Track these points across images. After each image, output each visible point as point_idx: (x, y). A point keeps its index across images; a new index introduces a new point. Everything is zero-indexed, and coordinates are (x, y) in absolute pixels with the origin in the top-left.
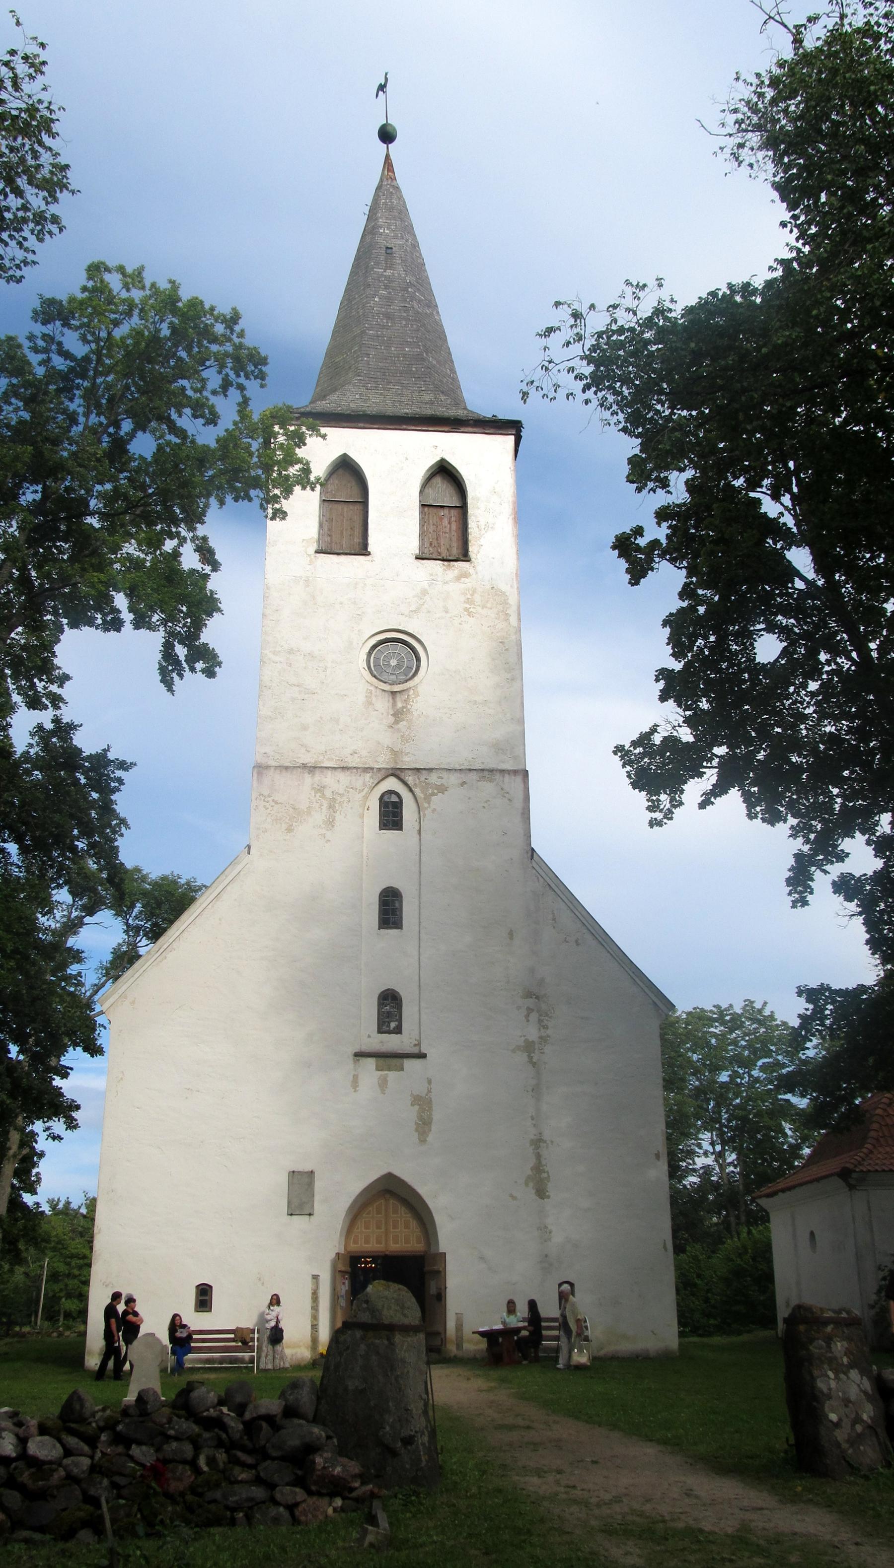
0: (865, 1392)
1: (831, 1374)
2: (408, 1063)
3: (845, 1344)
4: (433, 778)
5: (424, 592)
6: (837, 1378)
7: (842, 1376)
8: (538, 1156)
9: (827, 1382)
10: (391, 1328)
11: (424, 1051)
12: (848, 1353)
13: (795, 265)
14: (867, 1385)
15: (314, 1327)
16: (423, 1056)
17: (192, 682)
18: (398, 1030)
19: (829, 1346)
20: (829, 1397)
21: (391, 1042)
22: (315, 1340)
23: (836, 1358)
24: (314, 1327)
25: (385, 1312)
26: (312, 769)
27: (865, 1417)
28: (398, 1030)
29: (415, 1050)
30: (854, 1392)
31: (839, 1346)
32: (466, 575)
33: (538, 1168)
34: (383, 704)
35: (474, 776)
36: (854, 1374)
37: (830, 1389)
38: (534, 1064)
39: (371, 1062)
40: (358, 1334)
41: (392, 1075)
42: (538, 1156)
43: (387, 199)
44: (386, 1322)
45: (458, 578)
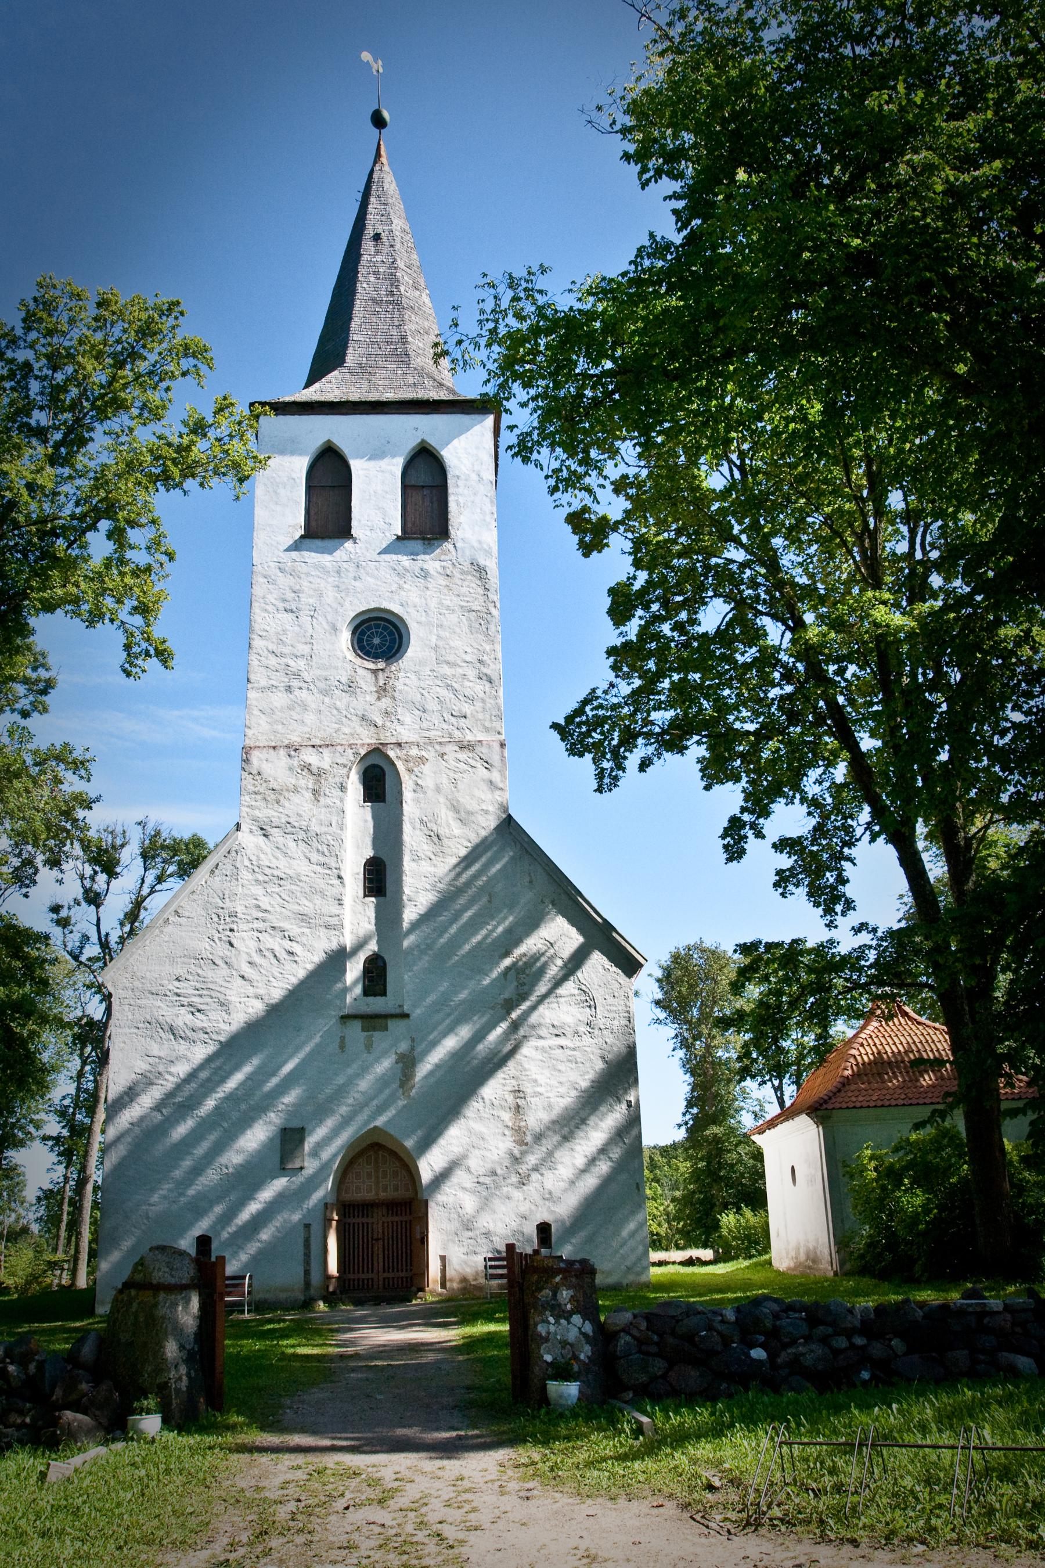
0: (585, 1335)
1: (551, 1319)
2: (391, 1024)
3: (571, 1292)
6: (557, 1322)
7: (563, 1321)
9: (547, 1326)
10: (158, 1288)
11: (406, 1009)
12: (572, 1299)
13: (978, 8)
14: (588, 1328)
15: (307, 1272)
16: (406, 1016)
17: (93, 768)
18: (384, 993)
19: (555, 1295)
20: (546, 1340)
21: (377, 1005)
22: (307, 1284)
23: (559, 1305)
24: (307, 1272)
25: (155, 1274)
27: (582, 1356)
28: (384, 993)
29: (398, 1011)
30: (572, 1335)
31: (565, 1294)
34: (366, 681)
36: (577, 1319)
37: (549, 1333)
39: (357, 1025)
40: (133, 1292)
41: (377, 1035)
44: (155, 1282)
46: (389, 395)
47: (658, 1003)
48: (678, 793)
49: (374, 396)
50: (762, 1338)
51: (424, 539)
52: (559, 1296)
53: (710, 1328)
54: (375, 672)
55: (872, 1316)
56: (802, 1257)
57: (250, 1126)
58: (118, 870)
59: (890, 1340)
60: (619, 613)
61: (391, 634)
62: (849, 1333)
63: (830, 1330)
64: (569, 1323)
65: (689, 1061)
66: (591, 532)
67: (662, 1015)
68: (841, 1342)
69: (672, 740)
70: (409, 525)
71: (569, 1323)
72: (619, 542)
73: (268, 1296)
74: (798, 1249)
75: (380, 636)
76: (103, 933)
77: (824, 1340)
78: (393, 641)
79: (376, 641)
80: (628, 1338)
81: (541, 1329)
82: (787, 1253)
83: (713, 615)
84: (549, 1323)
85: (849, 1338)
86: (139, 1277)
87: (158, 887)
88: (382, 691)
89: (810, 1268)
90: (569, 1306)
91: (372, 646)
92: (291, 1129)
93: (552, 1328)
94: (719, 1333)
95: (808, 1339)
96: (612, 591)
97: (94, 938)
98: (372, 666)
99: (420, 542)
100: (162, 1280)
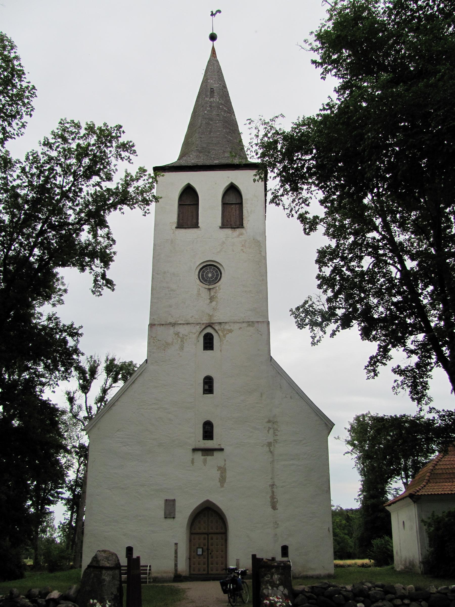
1: (270, 588)
2: (216, 453)
4: (227, 327)
5: (223, 243)
7: (275, 588)
8: (273, 492)
12: (280, 579)
14: (286, 592)
16: (222, 450)
19: (272, 577)
21: (209, 444)
26: (174, 325)
32: (242, 234)
33: (273, 497)
34: (205, 294)
35: (245, 325)
36: (281, 588)
37: (268, 593)
38: (271, 452)
39: (200, 453)
41: (209, 458)
42: (273, 492)
43: (214, 70)
45: (239, 236)
46: (216, 162)
47: (348, 442)
48: (352, 345)
49: (208, 163)
50: (362, 599)
51: (232, 228)
52: (273, 577)
53: (340, 593)
54: (209, 289)
55: (414, 591)
56: (408, 564)
57: (11, 581)
58: (96, 376)
59: (421, 602)
60: (321, 262)
61: (217, 272)
62: (402, 597)
63: (393, 596)
64: (278, 589)
65: (363, 469)
66: (310, 225)
67: (351, 448)
68: (398, 602)
69: (346, 323)
70: (225, 221)
71: (278, 589)
72: (321, 228)
73: (159, 575)
74: (406, 562)
75: (210, 273)
76: (88, 405)
77: (391, 600)
78: (217, 275)
79: (210, 275)
80: (303, 597)
81: (265, 591)
82: (401, 562)
83: (367, 262)
84: (268, 589)
85: (402, 601)
86: (94, 564)
87: (113, 385)
88: (212, 299)
89: (411, 569)
90: (278, 582)
91: (207, 277)
92: (169, 500)
93: (270, 592)
94: (344, 596)
95: (383, 599)
96: (319, 252)
97: (84, 408)
98: (207, 287)
99: (230, 229)
100: (104, 565)
